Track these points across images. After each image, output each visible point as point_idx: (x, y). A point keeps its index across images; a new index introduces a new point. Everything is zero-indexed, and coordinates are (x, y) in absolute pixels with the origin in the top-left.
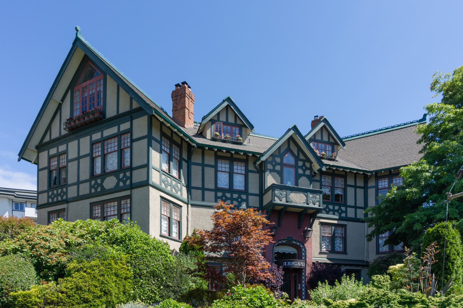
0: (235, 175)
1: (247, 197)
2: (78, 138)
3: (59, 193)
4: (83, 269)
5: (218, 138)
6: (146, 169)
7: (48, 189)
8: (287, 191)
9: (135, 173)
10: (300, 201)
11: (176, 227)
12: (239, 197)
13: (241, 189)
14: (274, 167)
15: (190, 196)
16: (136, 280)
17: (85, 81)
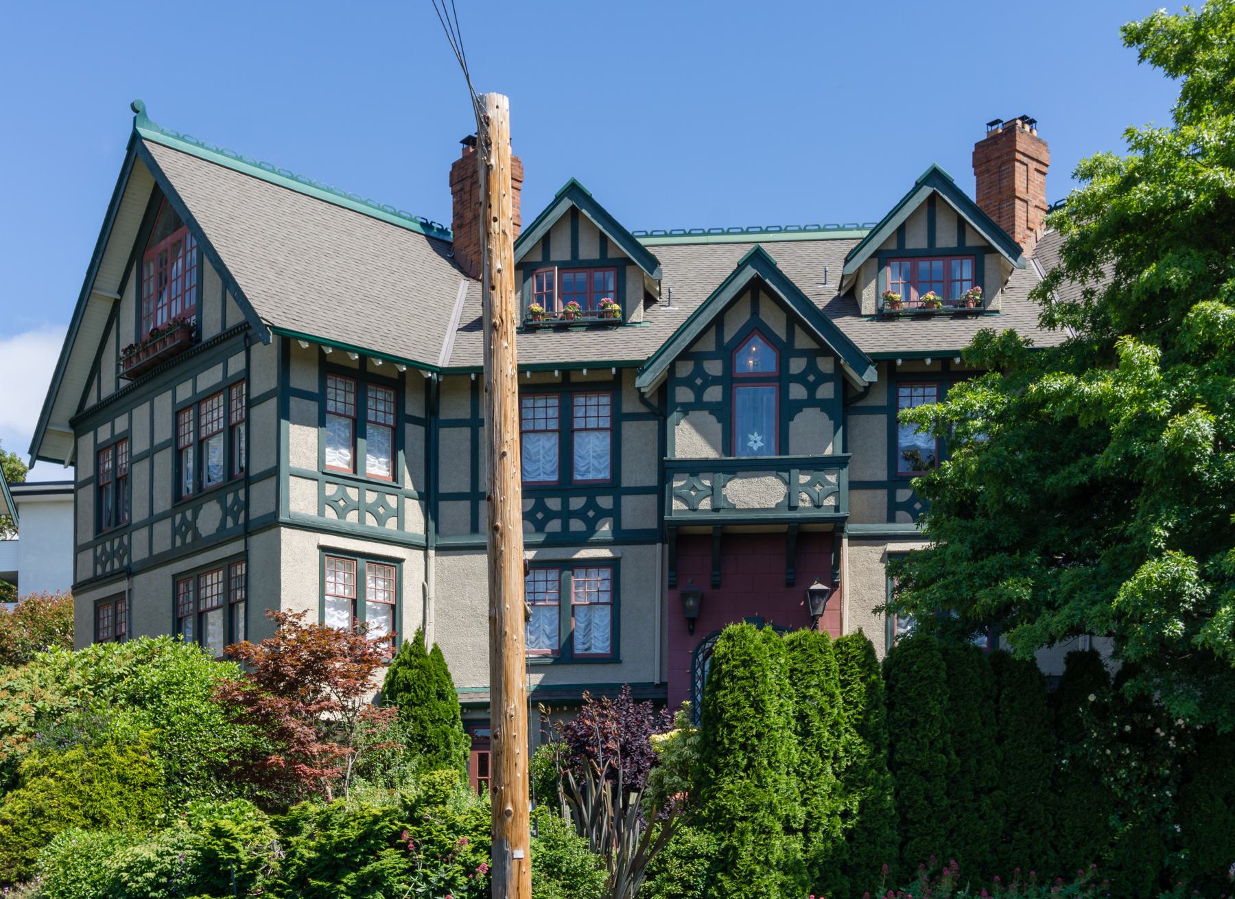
0: (578, 439)
1: (617, 503)
2: (149, 398)
3: (115, 548)
4: (48, 770)
5: (542, 320)
6: (274, 479)
7: (96, 539)
8: (717, 475)
9: (255, 490)
10: (763, 500)
11: (387, 621)
12: (591, 504)
13: (600, 477)
14: (699, 392)
15: (432, 525)
16: (173, 787)
17: (164, 237)
